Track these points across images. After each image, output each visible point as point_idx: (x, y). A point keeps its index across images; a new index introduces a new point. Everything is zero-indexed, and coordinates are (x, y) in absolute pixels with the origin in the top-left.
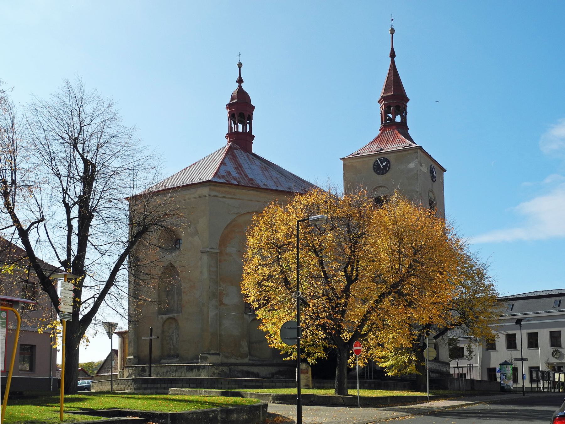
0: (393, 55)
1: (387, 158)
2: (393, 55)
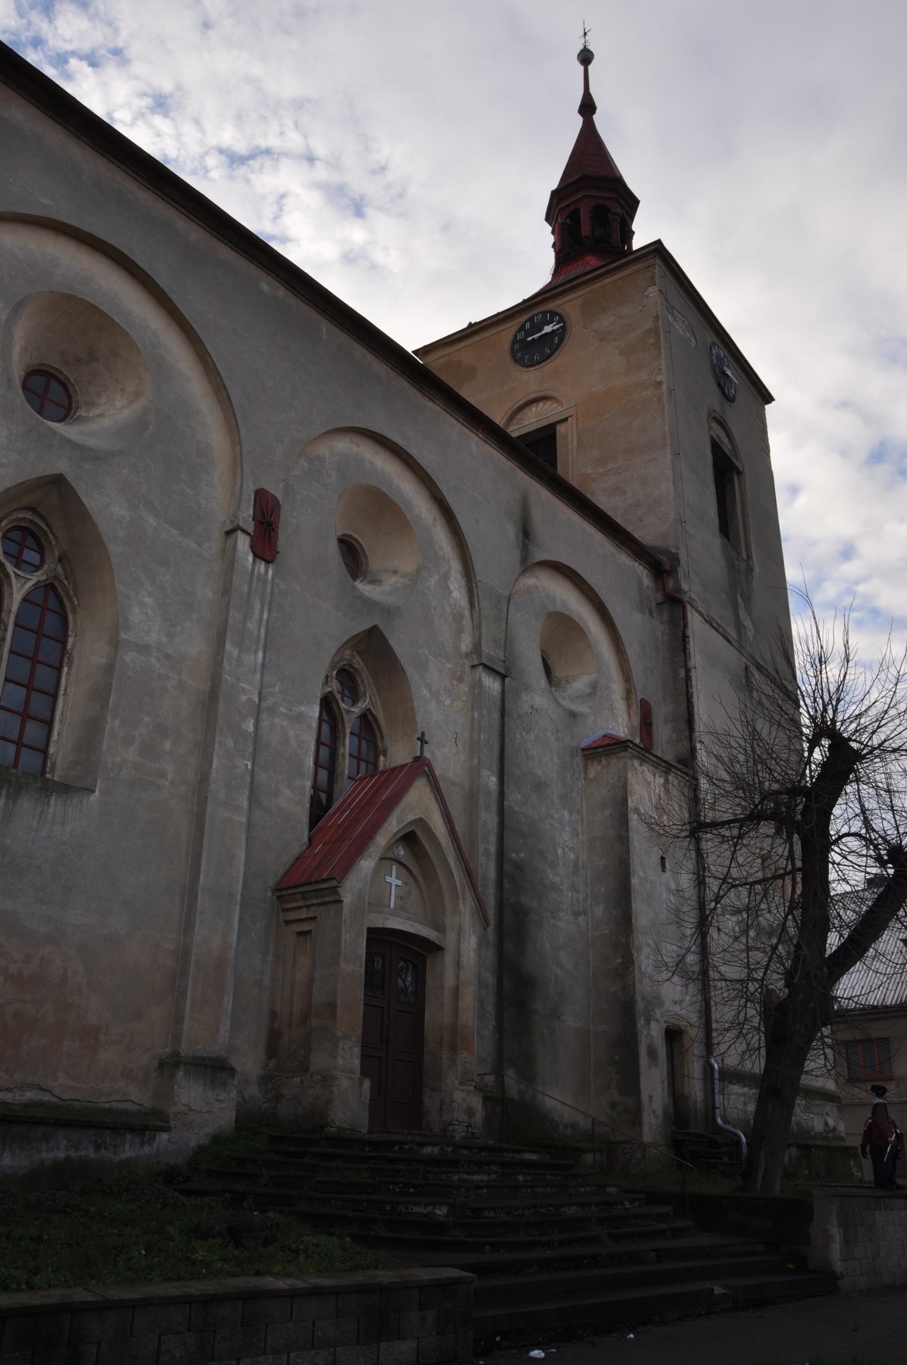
0: (588, 107)
1: (555, 310)
2: (588, 107)
